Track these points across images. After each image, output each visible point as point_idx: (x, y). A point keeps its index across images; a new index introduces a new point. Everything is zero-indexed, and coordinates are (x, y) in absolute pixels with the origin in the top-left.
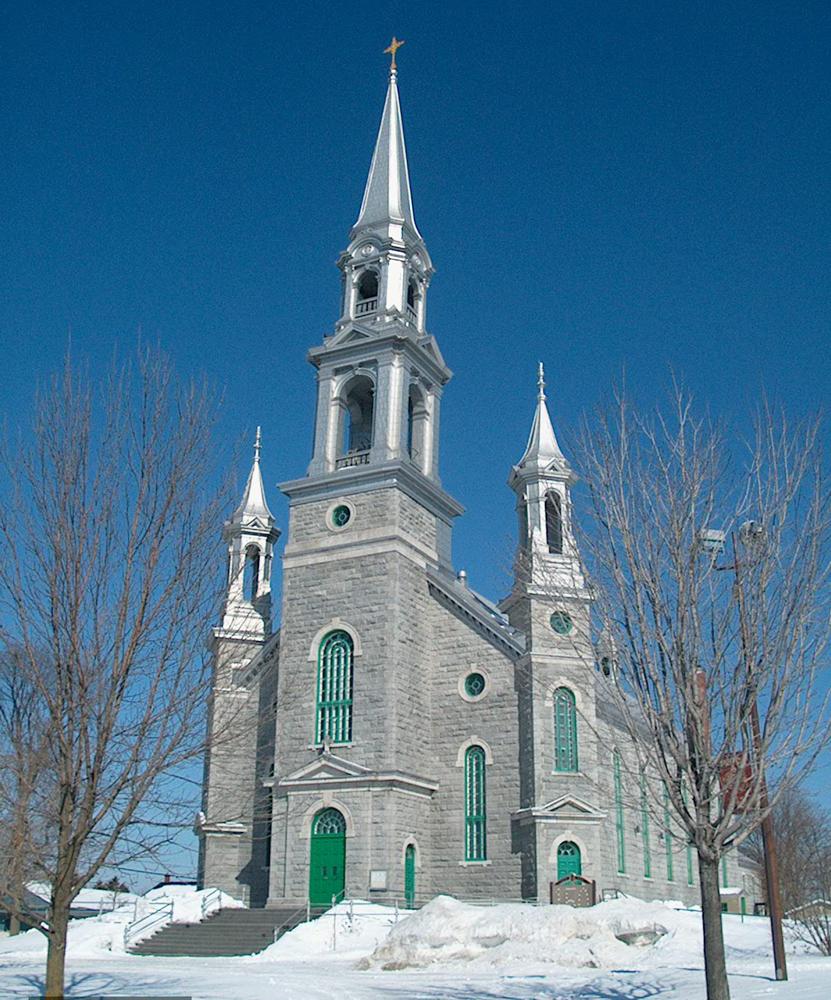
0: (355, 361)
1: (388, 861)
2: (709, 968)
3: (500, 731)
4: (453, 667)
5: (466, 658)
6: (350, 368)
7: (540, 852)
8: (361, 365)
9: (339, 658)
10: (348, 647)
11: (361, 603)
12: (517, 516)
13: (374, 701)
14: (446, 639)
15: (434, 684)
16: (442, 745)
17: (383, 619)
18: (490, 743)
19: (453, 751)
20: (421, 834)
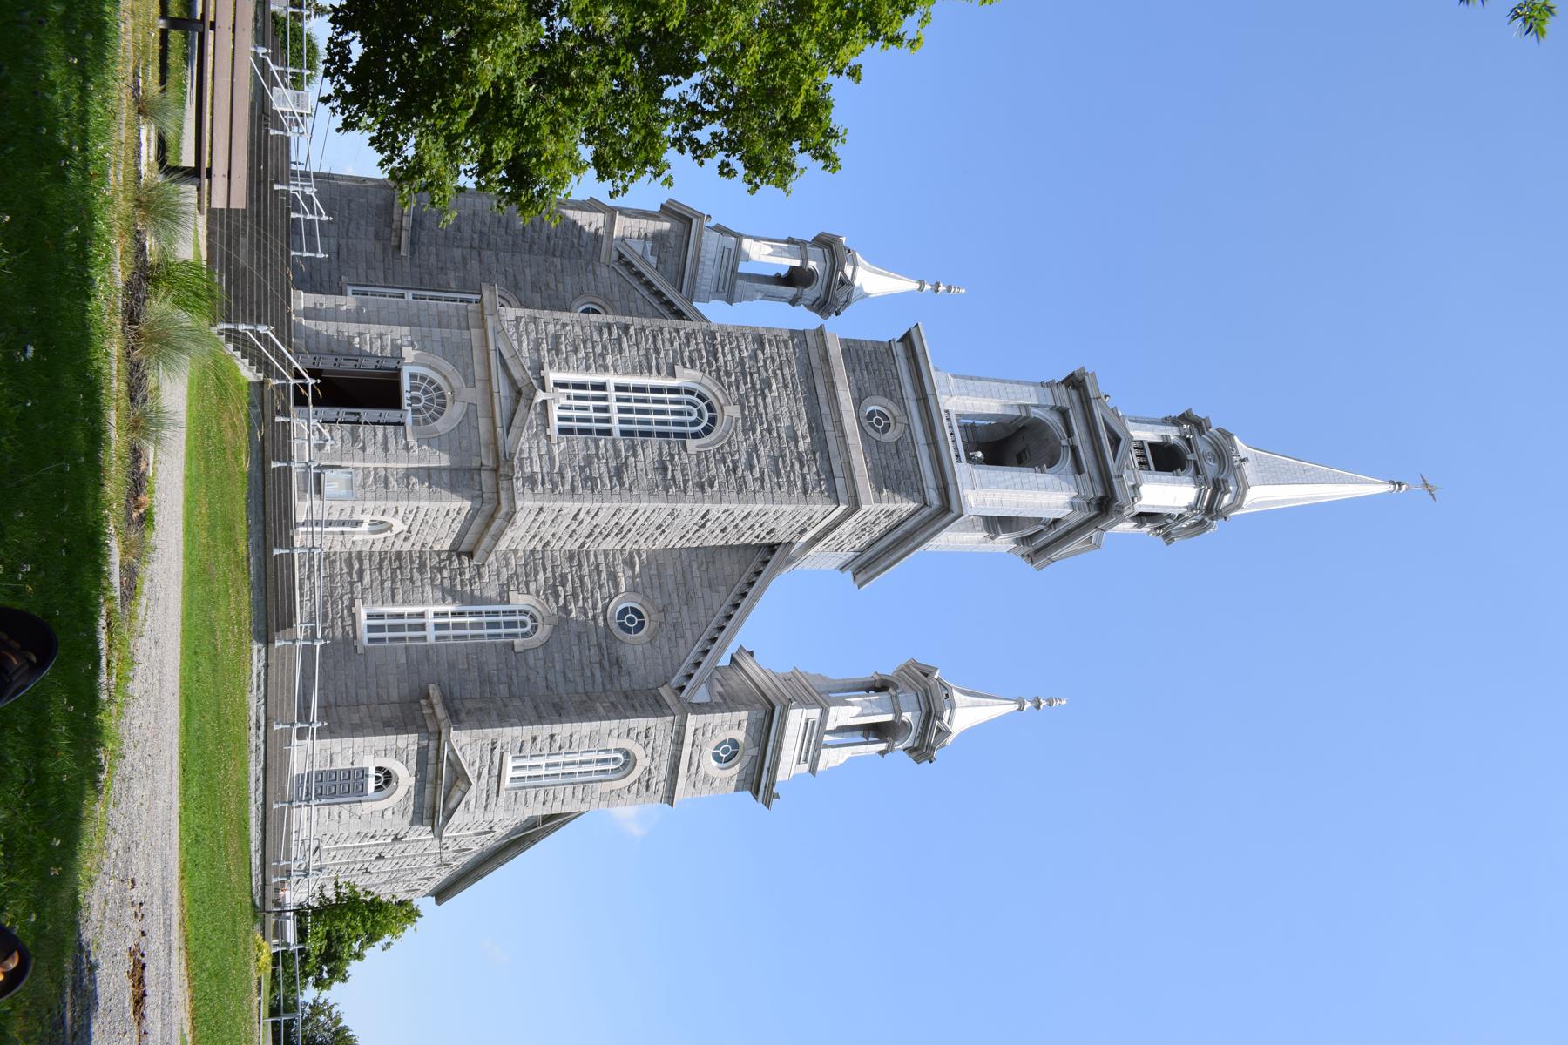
0: (1080, 436)
1: (462, 168)
2: (272, 763)
3: (564, 662)
4: (656, 584)
5: (671, 603)
6: (1070, 434)
7: (381, 741)
8: (1074, 450)
9: (680, 413)
10: (699, 428)
11: (762, 451)
12: (866, 673)
13: (618, 472)
14: (696, 573)
15: (631, 554)
16: (540, 568)
17: (741, 486)
18: (546, 645)
19: (532, 586)
20: (406, 539)
